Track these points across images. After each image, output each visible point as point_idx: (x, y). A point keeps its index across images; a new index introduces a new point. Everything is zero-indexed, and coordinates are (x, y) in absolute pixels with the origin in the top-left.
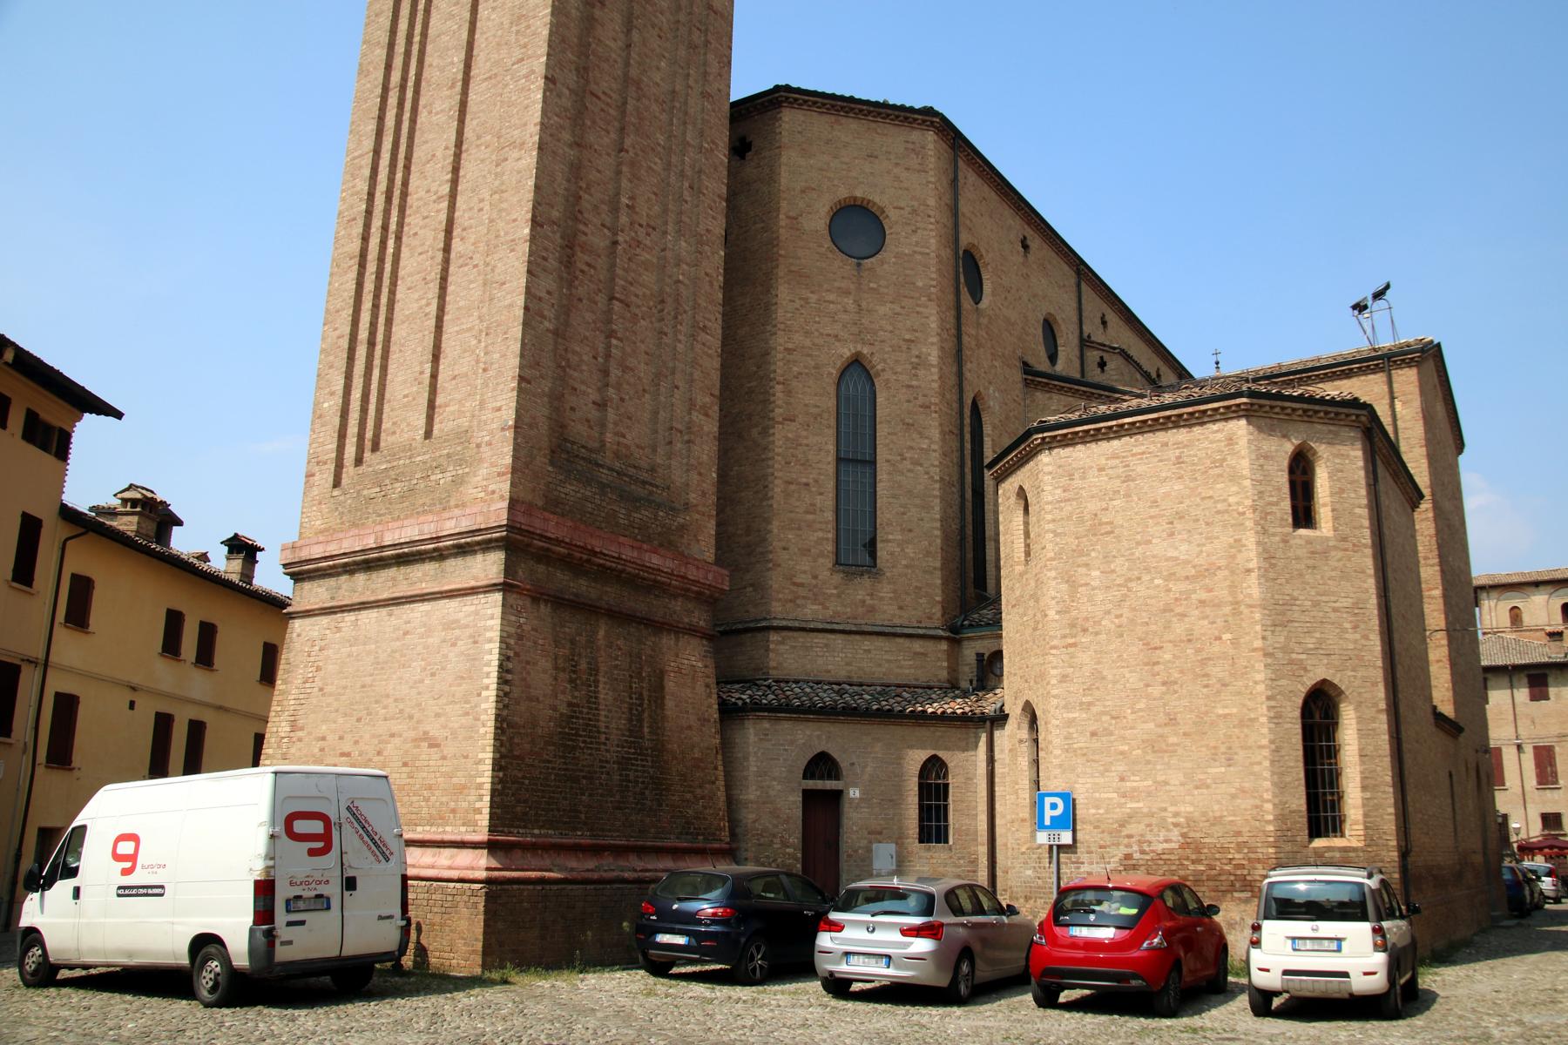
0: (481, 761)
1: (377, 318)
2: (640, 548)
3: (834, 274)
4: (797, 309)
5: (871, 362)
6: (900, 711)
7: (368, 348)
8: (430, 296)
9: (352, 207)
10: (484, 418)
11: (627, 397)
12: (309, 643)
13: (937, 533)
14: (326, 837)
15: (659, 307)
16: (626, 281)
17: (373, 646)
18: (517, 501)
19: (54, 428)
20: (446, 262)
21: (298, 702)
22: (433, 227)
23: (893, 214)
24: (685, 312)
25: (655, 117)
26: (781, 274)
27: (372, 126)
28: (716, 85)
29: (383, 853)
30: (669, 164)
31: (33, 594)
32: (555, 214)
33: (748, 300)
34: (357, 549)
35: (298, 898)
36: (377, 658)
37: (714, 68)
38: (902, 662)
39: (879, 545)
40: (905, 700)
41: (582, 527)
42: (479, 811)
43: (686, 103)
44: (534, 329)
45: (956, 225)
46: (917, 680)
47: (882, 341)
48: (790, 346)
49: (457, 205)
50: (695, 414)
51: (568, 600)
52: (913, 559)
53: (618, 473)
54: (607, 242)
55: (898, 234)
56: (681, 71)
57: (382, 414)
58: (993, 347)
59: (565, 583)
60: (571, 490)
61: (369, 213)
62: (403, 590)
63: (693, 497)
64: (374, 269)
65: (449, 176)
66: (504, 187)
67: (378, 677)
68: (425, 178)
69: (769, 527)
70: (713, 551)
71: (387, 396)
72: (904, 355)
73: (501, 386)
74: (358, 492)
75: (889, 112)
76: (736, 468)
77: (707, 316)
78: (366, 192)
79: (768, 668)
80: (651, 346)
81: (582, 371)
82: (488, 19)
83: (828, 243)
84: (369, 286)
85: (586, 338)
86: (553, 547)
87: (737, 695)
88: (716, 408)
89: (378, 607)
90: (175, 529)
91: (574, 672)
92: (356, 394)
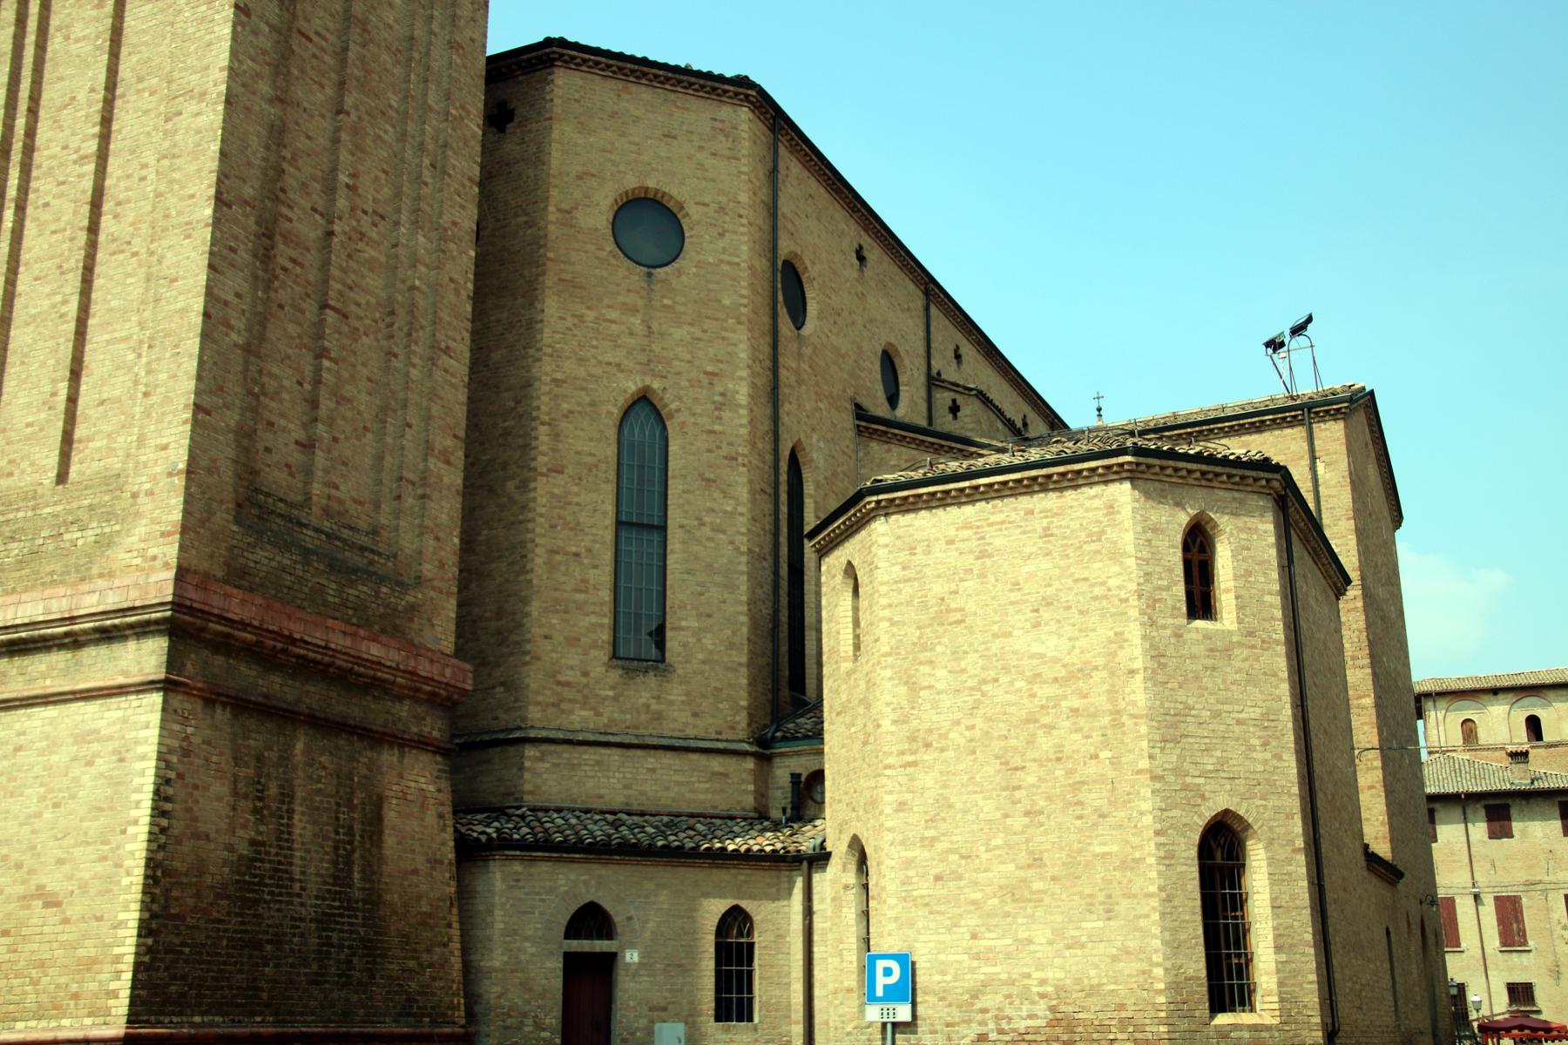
0: (121, 924)
2: (354, 635)
3: (618, 285)
5: (662, 399)
6: (692, 848)
8: (68, 290)
11: (342, 437)
13: (744, 619)
15: (388, 320)
16: (344, 284)
18: (187, 570)
20: (92, 245)
23: (694, 211)
24: (422, 328)
26: (549, 283)
28: (468, 33)
32: (248, 191)
39: (669, 634)
40: (699, 834)
41: (278, 605)
42: (114, 994)
43: (428, 53)
44: (215, 342)
45: (774, 229)
46: (714, 807)
48: (559, 376)
49: (110, 169)
52: (711, 652)
54: (319, 233)
59: (251, 680)
60: (263, 558)
63: (428, 569)
65: (97, 129)
66: (176, 151)
75: (693, 80)
83: (610, 246)
85: (288, 357)
86: (236, 633)
88: (461, 454)
91: (260, 799)
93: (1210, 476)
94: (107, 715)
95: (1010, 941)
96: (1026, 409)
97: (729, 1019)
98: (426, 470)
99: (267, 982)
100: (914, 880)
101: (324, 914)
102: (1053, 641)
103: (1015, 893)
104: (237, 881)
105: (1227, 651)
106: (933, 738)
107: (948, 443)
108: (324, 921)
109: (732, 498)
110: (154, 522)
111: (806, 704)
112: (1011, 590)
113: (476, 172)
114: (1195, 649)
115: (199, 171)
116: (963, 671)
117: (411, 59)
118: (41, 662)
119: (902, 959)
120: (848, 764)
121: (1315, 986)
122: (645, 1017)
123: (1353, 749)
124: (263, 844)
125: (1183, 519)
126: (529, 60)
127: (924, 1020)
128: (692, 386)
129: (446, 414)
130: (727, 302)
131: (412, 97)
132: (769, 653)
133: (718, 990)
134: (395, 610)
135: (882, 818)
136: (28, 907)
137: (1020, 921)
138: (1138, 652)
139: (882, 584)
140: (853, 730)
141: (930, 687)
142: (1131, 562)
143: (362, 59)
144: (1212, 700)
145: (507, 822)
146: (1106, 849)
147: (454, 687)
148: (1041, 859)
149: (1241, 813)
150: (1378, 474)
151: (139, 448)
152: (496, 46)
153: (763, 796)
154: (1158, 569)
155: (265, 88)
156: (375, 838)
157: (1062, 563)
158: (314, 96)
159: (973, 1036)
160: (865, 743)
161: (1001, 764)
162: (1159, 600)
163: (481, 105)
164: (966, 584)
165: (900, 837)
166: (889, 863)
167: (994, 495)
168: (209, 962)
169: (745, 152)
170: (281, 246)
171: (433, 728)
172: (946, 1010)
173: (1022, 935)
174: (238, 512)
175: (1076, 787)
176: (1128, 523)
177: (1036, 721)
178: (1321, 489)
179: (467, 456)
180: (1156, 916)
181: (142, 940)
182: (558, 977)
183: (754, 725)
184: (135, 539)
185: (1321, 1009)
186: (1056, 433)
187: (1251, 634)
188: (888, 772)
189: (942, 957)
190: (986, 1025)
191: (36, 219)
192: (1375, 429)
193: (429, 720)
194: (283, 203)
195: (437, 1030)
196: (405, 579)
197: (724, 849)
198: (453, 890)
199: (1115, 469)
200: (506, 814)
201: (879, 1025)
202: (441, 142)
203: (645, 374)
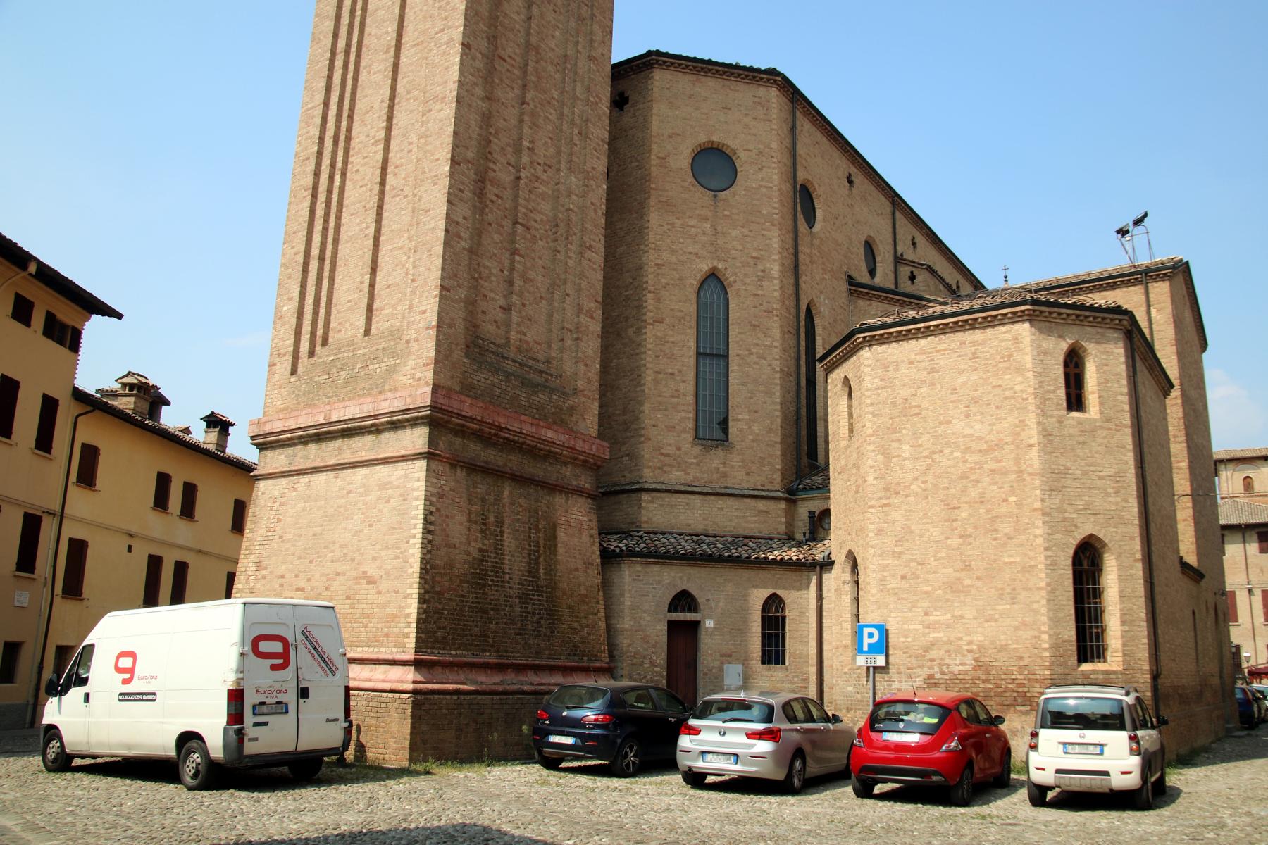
0: (408, 596)
1: (326, 238)
2: (537, 425)
3: (695, 203)
4: (664, 232)
5: (724, 275)
6: (747, 558)
8: (369, 220)
11: (528, 303)
13: (778, 413)
14: (285, 655)
15: (554, 230)
16: (527, 209)
17: (323, 503)
18: (439, 386)
19: (68, 326)
20: (382, 193)
23: (743, 155)
24: (575, 234)
26: (652, 204)
27: (323, 83)
28: (600, 50)
29: (330, 669)
32: (470, 155)
35: (263, 704)
37: (598, 37)
38: (749, 518)
39: (731, 423)
40: (751, 548)
41: (491, 407)
42: (407, 636)
43: (576, 65)
44: (452, 247)
45: (794, 164)
46: (760, 532)
48: (659, 262)
49: (391, 147)
52: (758, 435)
53: (520, 364)
54: (512, 178)
57: (330, 316)
59: (476, 453)
60: (482, 378)
61: (320, 154)
63: (580, 384)
65: (385, 124)
66: (429, 133)
71: (334, 301)
75: (741, 72)
78: (317, 137)
83: (690, 179)
84: (320, 213)
85: (495, 255)
86: (467, 424)
88: (600, 312)
89: (327, 471)
90: (164, 407)
91: (484, 524)
92: (309, 300)
93: (1082, 318)
94: (396, 473)
95: (949, 617)
96: (959, 277)
97: (770, 662)
98: (579, 322)
99: (492, 633)
100: (888, 578)
101: (523, 594)
102: (978, 426)
103: (953, 587)
104: (473, 573)
105: (1093, 432)
106: (900, 488)
107: (909, 300)
108: (524, 598)
109: (770, 337)
110: (419, 357)
111: (817, 467)
112: (952, 394)
113: (606, 135)
114: (1071, 431)
115: (441, 144)
116: (920, 446)
117: (565, 68)
118: (359, 441)
119: (880, 627)
120: (846, 505)
121: (1147, 646)
122: (718, 660)
123: (1174, 495)
124: (486, 551)
125: (1064, 346)
126: (638, 65)
127: (894, 665)
128: (743, 266)
129: (591, 287)
130: (765, 212)
131: (567, 92)
132: (794, 435)
133: (763, 645)
134: (561, 409)
135: (868, 539)
136: (359, 584)
137: (956, 604)
138: (1034, 432)
139: (868, 390)
140: (849, 483)
141: (899, 456)
142: (1030, 374)
143: (536, 70)
144: (1083, 464)
145: (632, 540)
146: (1012, 559)
147: (598, 457)
148: (970, 566)
149: (1101, 536)
150: (1191, 316)
151: (409, 313)
152: (617, 57)
153: (791, 525)
154: (1048, 379)
155: (479, 91)
156: (552, 549)
157: (984, 376)
158: (508, 95)
159: (924, 675)
160: (857, 492)
161: (945, 505)
162: (1047, 399)
163: (609, 95)
164: (922, 390)
165: (879, 552)
166: (872, 567)
167: (949, 330)
168: (459, 620)
169: (775, 116)
170: (489, 187)
171: (585, 482)
172: (909, 659)
173: (956, 613)
174: (467, 351)
175: (993, 520)
176: (1028, 349)
177: (968, 478)
178: (1154, 326)
179: (603, 314)
180: (1044, 602)
181: (420, 605)
182: (664, 635)
183: (785, 481)
185: (1150, 661)
186: (978, 292)
187: (1108, 421)
188: (871, 510)
189: (906, 627)
190: (933, 669)
191: (351, 180)
192: (1189, 282)
193: (583, 477)
194: (490, 161)
195: (592, 665)
196: (567, 390)
197: (766, 558)
198: (599, 581)
199: (1019, 314)
200: (631, 535)
201: (865, 668)
202: (584, 118)
203: (713, 259)
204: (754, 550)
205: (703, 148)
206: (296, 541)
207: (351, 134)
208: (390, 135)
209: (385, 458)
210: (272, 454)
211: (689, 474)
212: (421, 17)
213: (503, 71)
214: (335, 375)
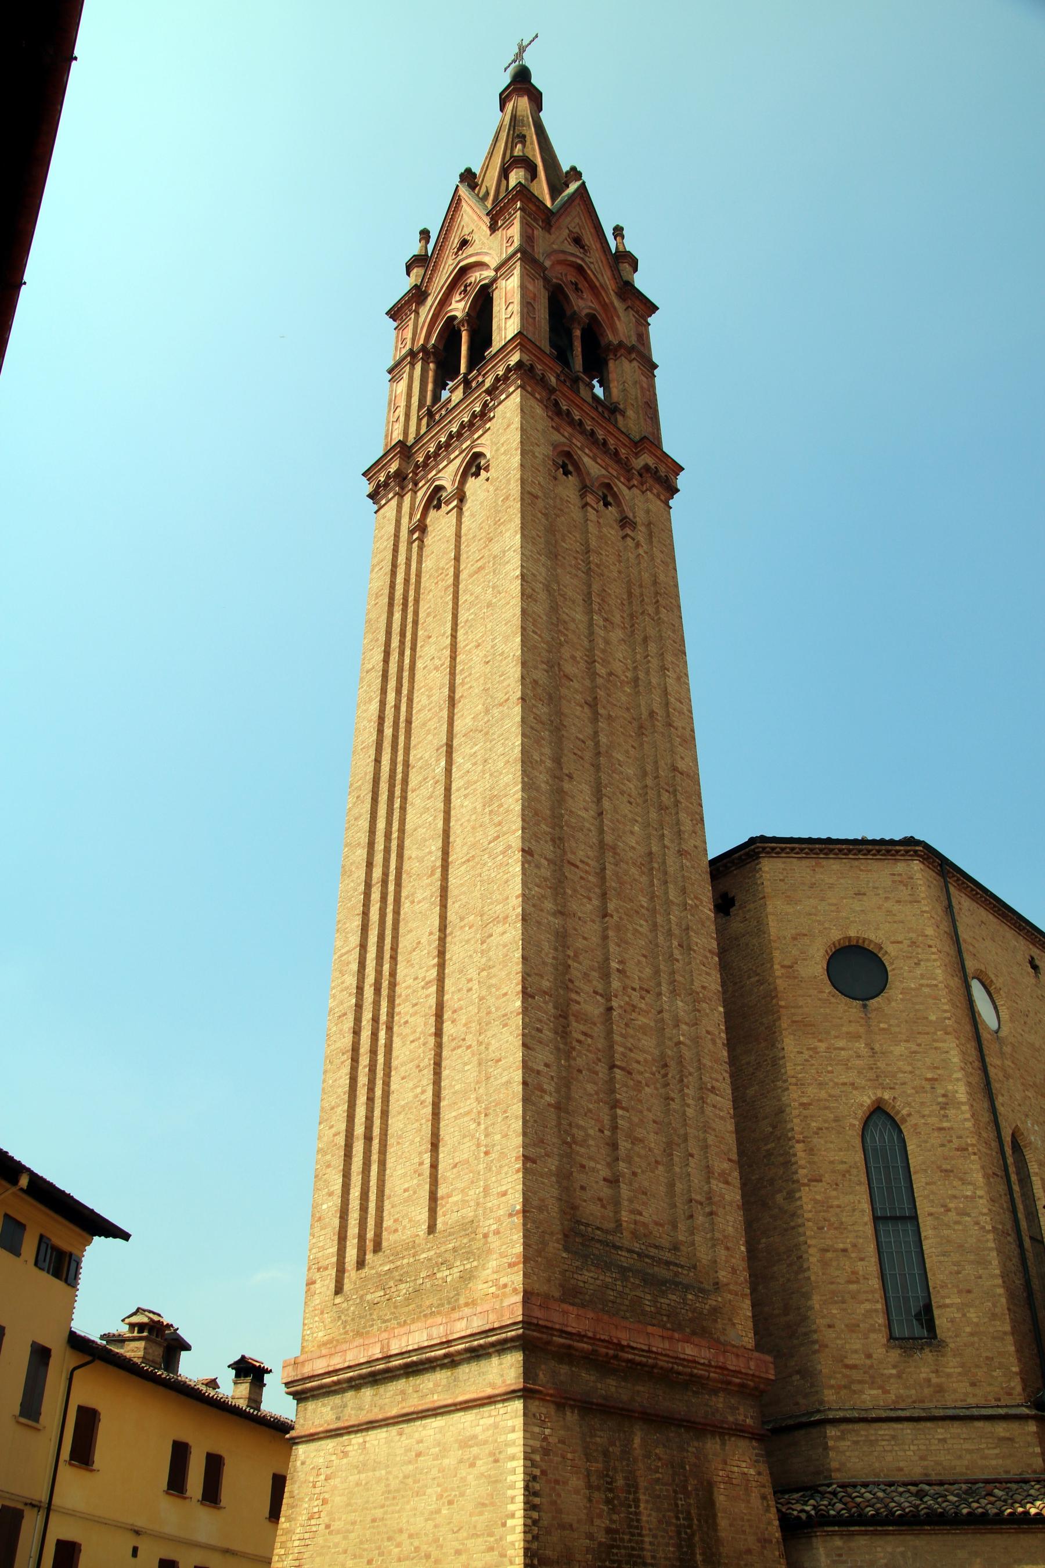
1: (373, 1112)
2: (671, 1338)
3: (841, 1018)
4: (806, 1060)
5: (894, 1107)
6: (997, 1514)
7: (365, 1143)
8: (425, 1082)
9: (342, 1003)
10: (489, 1205)
11: (639, 1171)
12: (315, 1472)
13: (1000, 1291)
15: (663, 1072)
16: (626, 1048)
17: (383, 1472)
18: (532, 1294)
19: (65, 1253)
20: (439, 1046)
21: (303, 1543)
22: (423, 1013)
23: (891, 949)
24: (690, 1074)
25: (635, 880)
26: (784, 1025)
27: (357, 922)
28: (692, 842)
30: (655, 925)
31: (39, 1430)
32: (546, 984)
33: (753, 1058)
34: (362, 1360)
36: (388, 1485)
37: (687, 826)
38: (986, 1451)
39: (936, 1312)
40: (999, 1499)
41: (606, 1317)
43: (664, 863)
44: (534, 1104)
45: (960, 952)
46: (1007, 1472)
47: (904, 1084)
48: (805, 1100)
49: (446, 988)
50: (714, 1182)
51: (597, 1404)
52: (977, 1325)
53: (638, 1254)
54: (602, 1010)
55: (902, 968)
56: (655, 832)
57: (382, 1212)
58: (1022, 1076)
59: (592, 1384)
60: (589, 1278)
61: (359, 1007)
62: (413, 1403)
63: (723, 1275)
64: (367, 1062)
65: (436, 961)
66: (491, 963)
67: (389, 1509)
68: (412, 965)
69: (810, 1303)
70: (751, 1335)
71: (387, 1192)
72: (929, 1095)
73: (506, 1169)
74: (361, 1297)
75: (870, 847)
76: (764, 1240)
77: (714, 1076)
79: (830, 1470)
80: (659, 1114)
81: (588, 1146)
82: (462, 806)
83: (829, 988)
84: (363, 1079)
85: (590, 1111)
86: (576, 1344)
87: (799, 1507)
88: (736, 1174)
89: (387, 1425)
90: (183, 1354)
91: (611, 1490)
92: (355, 1193)
94: (482, 1422)
110: (502, 1255)
113: (714, 944)
117: (652, 869)
124: (616, 1531)
128: (917, 1092)
129: (720, 1142)
130: (933, 1018)
134: (701, 1313)
143: (616, 874)
151: (485, 1197)
155: (549, 905)
170: (574, 1024)
171: (746, 1416)
174: (565, 1242)
184: (489, 1271)
193: (742, 1410)
194: (572, 990)
202: (684, 927)
203: (876, 1088)
204: (1005, 1501)
205: (838, 947)
206: (348, 1531)
207: (395, 979)
208: (444, 974)
209: (466, 1402)
210: (314, 1406)
211: (888, 1392)
212: (469, 828)
213: (576, 879)
214: (393, 1290)
